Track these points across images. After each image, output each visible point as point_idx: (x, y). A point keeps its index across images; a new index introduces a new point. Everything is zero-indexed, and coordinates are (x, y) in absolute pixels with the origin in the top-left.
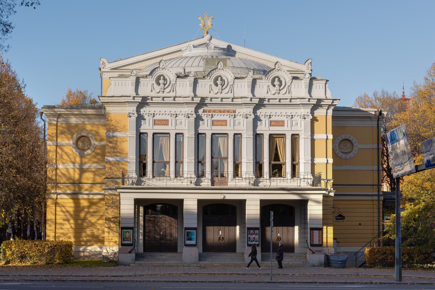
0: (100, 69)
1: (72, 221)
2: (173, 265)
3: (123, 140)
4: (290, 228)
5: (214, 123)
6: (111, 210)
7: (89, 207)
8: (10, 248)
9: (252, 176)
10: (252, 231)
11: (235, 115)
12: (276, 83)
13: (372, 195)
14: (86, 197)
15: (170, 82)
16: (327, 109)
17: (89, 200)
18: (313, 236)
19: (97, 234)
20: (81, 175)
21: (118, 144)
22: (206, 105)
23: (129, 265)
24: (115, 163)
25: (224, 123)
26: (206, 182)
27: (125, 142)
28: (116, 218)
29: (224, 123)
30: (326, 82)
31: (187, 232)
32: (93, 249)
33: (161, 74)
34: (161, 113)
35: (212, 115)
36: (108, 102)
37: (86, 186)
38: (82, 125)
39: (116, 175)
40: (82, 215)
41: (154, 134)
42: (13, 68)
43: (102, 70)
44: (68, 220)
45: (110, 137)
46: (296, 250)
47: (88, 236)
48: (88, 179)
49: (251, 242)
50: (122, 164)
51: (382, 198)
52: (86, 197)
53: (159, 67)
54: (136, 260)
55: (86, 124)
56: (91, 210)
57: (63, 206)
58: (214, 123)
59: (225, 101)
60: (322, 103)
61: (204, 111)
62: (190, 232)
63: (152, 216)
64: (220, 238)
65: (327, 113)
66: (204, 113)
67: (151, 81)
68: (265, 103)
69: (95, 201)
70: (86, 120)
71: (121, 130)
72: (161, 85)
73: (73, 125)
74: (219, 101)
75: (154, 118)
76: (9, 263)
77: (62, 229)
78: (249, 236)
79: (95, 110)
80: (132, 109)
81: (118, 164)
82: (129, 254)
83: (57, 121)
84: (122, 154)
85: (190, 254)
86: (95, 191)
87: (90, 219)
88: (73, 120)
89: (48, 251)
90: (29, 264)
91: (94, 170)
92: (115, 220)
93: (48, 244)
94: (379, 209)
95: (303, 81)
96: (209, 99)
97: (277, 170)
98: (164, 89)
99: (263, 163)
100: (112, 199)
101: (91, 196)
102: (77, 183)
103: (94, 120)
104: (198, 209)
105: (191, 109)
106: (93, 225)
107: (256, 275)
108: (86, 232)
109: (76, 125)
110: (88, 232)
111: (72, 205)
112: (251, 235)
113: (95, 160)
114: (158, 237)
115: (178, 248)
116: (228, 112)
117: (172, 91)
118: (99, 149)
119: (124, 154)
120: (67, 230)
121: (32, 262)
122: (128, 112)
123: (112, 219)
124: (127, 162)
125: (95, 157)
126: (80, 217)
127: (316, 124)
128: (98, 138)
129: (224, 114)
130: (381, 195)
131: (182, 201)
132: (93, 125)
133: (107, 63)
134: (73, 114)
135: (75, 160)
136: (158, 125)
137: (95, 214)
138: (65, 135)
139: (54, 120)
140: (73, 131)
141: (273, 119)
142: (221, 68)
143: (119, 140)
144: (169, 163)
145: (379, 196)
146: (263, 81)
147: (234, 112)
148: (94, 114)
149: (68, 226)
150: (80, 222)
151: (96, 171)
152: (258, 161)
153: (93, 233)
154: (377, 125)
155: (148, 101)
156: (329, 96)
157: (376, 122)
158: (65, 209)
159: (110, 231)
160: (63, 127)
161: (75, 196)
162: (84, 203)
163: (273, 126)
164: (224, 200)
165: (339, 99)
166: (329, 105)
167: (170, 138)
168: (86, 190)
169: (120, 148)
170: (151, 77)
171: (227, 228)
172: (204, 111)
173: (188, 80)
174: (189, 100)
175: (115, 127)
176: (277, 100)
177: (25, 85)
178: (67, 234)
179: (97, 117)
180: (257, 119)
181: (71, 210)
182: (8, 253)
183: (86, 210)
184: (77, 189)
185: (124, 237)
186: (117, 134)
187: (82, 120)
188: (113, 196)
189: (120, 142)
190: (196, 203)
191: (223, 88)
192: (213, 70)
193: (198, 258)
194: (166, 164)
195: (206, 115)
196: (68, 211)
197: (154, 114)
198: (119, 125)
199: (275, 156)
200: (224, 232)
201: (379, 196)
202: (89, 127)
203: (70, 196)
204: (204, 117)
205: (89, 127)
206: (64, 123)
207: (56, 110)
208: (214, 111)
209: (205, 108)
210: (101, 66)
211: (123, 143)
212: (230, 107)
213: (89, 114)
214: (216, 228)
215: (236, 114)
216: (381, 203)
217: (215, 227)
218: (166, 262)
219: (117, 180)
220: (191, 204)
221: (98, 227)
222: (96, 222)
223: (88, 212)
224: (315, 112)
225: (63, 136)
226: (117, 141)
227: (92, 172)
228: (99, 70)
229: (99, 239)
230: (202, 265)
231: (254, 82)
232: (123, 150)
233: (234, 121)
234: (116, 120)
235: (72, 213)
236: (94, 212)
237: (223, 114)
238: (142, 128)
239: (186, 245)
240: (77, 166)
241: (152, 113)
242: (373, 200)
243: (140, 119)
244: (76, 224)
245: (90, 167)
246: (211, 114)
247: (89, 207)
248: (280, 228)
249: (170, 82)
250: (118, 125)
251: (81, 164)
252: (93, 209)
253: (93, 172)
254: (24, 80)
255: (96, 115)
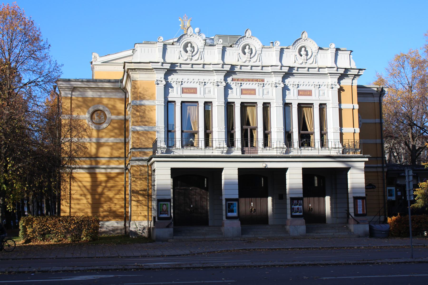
0: (92, 63)
1: (89, 196)
2: (216, 240)
3: (152, 109)
4: (322, 198)
5: (243, 92)
6: (139, 182)
7: (106, 182)
8: (31, 225)
9: (282, 144)
10: (295, 202)
11: (263, 84)
12: (303, 52)
13: (376, 167)
14: (103, 171)
15: (198, 50)
16: (353, 79)
17: (106, 174)
18: (357, 205)
19: (114, 209)
20: (97, 149)
21: (147, 112)
22: (235, 73)
23: (167, 240)
24: (143, 133)
25: (253, 92)
26: (237, 151)
27: (154, 111)
28: (145, 190)
29: (252, 92)
30: (351, 53)
31: (228, 203)
32: (110, 225)
33: (189, 41)
34: (189, 81)
35: (241, 83)
36: (135, 69)
37: (103, 161)
38: (98, 99)
39: (144, 145)
40: (100, 190)
41: (182, 102)
42: (37, 24)
43: (93, 63)
44: (85, 195)
45: (137, 106)
46: (270, 222)
47: (106, 211)
48: (105, 153)
49: (295, 213)
50: (151, 133)
51: (386, 170)
52: (103, 171)
53: (187, 34)
54: (174, 236)
55: (102, 98)
56: (109, 185)
57: (80, 181)
58: (243, 92)
59: (255, 69)
60: (349, 73)
61: (233, 80)
62: (232, 204)
63: (182, 188)
64: (252, 209)
65: (352, 83)
66: (233, 82)
67: (179, 47)
68: (294, 72)
69: (112, 175)
70: (103, 93)
71: (149, 98)
72: (189, 52)
73: (90, 99)
74: (248, 69)
75: (182, 86)
76: (30, 242)
77: (78, 204)
78: (293, 207)
79: (112, 84)
80: (160, 76)
81: (147, 134)
82: (167, 230)
83: (72, 95)
84: (151, 123)
85: (231, 227)
86: (112, 166)
87: (107, 193)
88: (90, 94)
89: (74, 227)
90: (52, 242)
91: (111, 144)
92: (144, 192)
93: (74, 220)
94: (383, 180)
95: (329, 51)
96: (239, 67)
97: (305, 140)
98: (192, 56)
99: (292, 132)
100: (141, 171)
101: (109, 171)
102: (95, 157)
103: (111, 94)
104: (238, 179)
105: (220, 77)
106: (110, 199)
107: (319, 249)
108: (103, 207)
109: (93, 99)
110: (106, 207)
111: (89, 179)
112: (295, 205)
113: (113, 134)
114: (189, 210)
115: (209, 221)
116: (257, 80)
117: (200, 58)
118: (117, 123)
119: (153, 123)
120: (83, 205)
121: (56, 240)
122: (155, 80)
123: (141, 192)
124: (155, 131)
125: (112, 131)
126: (97, 192)
127: (342, 93)
128: (115, 112)
129: (253, 82)
130: (385, 167)
131: (221, 170)
132: (110, 99)
133: (98, 57)
134: (90, 87)
135: (91, 134)
136: (186, 93)
137: (113, 189)
138: (81, 109)
139: (69, 94)
140: (89, 104)
141: (301, 88)
142: (249, 37)
143: (147, 109)
144: (197, 132)
145: (383, 167)
146: (291, 51)
147: (263, 81)
148: (111, 88)
149: (85, 201)
150: (97, 197)
151: (114, 145)
152: (287, 130)
153: (110, 208)
154: (379, 101)
155: (177, 68)
156: (353, 66)
157: (378, 98)
158: (82, 183)
159: (139, 204)
160: (79, 101)
161: (92, 171)
162: (101, 178)
163: (301, 95)
164: (266, 170)
165: (365, 69)
166: (355, 75)
167: (198, 107)
168: (104, 164)
169: (149, 117)
170: (178, 44)
171: (258, 199)
172: (233, 80)
173: (217, 48)
174: (219, 67)
175: (143, 95)
176: (306, 69)
177: (50, 45)
178: (84, 210)
179: (114, 91)
180: (285, 89)
181: (88, 185)
182: (29, 230)
183: (104, 184)
184: (94, 164)
185: (161, 210)
186: (145, 102)
187: (99, 94)
188: (141, 167)
189: (149, 110)
190: (236, 172)
191: (251, 57)
192: (241, 38)
193: (240, 231)
194: (193, 135)
195: (235, 84)
196: (85, 186)
197: (182, 82)
198: (147, 93)
199: (303, 125)
200: (255, 204)
201: (383, 167)
202: (105, 101)
203: (87, 171)
204: (233, 86)
205: (105, 101)
206: (81, 96)
207: (72, 83)
208: (243, 80)
209: (234, 76)
210: (93, 60)
211: (151, 112)
212: (258, 75)
213: (105, 88)
214: (248, 200)
215: (265, 83)
216: (385, 174)
217: (246, 199)
218: (207, 237)
219: (145, 150)
220: (230, 173)
221: (116, 202)
222: (113, 197)
223: (106, 187)
224: (341, 82)
225: (79, 110)
226: (145, 109)
227: (108, 146)
228: (90, 64)
229: (117, 214)
230: (246, 239)
231: (282, 51)
232: (151, 119)
233: (263, 90)
234: (144, 88)
235: (89, 187)
236: (112, 187)
237: (251, 83)
238: (169, 96)
239: (228, 218)
240: (94, 140)
241: (180, 80)
242: (377, 172)
243: (168, 86)
244: (93, 199)
245: (106, 141)
246: (240, 82)
247: (106, 182)
248: (311, 199)
249: (198, 50)
250: (145, 93)
251: (98, 138)
252: (111, 183)
253: (111, 146)
254: (48, 41)
255: (113, 88)
